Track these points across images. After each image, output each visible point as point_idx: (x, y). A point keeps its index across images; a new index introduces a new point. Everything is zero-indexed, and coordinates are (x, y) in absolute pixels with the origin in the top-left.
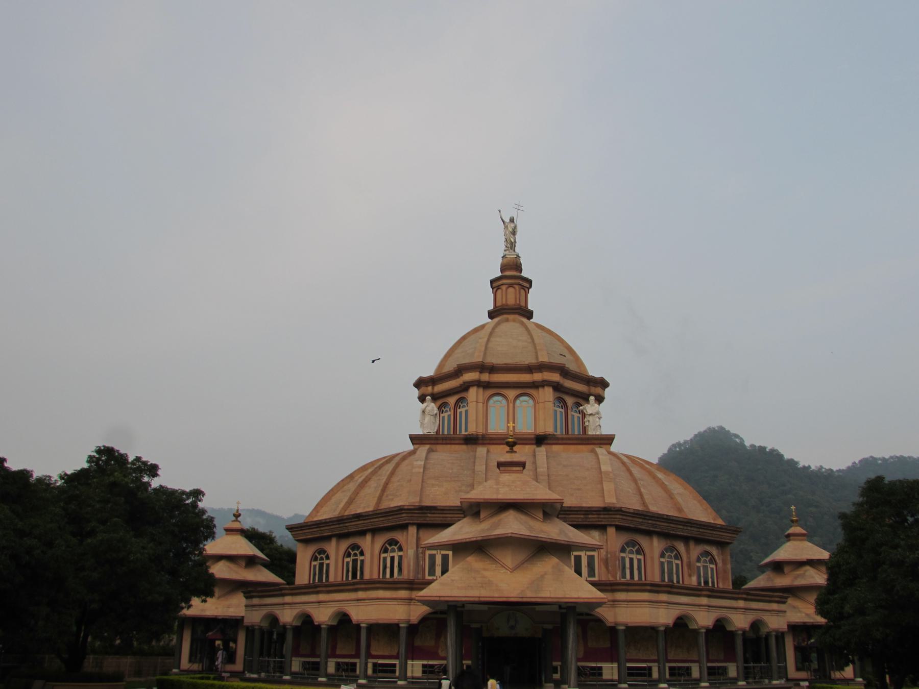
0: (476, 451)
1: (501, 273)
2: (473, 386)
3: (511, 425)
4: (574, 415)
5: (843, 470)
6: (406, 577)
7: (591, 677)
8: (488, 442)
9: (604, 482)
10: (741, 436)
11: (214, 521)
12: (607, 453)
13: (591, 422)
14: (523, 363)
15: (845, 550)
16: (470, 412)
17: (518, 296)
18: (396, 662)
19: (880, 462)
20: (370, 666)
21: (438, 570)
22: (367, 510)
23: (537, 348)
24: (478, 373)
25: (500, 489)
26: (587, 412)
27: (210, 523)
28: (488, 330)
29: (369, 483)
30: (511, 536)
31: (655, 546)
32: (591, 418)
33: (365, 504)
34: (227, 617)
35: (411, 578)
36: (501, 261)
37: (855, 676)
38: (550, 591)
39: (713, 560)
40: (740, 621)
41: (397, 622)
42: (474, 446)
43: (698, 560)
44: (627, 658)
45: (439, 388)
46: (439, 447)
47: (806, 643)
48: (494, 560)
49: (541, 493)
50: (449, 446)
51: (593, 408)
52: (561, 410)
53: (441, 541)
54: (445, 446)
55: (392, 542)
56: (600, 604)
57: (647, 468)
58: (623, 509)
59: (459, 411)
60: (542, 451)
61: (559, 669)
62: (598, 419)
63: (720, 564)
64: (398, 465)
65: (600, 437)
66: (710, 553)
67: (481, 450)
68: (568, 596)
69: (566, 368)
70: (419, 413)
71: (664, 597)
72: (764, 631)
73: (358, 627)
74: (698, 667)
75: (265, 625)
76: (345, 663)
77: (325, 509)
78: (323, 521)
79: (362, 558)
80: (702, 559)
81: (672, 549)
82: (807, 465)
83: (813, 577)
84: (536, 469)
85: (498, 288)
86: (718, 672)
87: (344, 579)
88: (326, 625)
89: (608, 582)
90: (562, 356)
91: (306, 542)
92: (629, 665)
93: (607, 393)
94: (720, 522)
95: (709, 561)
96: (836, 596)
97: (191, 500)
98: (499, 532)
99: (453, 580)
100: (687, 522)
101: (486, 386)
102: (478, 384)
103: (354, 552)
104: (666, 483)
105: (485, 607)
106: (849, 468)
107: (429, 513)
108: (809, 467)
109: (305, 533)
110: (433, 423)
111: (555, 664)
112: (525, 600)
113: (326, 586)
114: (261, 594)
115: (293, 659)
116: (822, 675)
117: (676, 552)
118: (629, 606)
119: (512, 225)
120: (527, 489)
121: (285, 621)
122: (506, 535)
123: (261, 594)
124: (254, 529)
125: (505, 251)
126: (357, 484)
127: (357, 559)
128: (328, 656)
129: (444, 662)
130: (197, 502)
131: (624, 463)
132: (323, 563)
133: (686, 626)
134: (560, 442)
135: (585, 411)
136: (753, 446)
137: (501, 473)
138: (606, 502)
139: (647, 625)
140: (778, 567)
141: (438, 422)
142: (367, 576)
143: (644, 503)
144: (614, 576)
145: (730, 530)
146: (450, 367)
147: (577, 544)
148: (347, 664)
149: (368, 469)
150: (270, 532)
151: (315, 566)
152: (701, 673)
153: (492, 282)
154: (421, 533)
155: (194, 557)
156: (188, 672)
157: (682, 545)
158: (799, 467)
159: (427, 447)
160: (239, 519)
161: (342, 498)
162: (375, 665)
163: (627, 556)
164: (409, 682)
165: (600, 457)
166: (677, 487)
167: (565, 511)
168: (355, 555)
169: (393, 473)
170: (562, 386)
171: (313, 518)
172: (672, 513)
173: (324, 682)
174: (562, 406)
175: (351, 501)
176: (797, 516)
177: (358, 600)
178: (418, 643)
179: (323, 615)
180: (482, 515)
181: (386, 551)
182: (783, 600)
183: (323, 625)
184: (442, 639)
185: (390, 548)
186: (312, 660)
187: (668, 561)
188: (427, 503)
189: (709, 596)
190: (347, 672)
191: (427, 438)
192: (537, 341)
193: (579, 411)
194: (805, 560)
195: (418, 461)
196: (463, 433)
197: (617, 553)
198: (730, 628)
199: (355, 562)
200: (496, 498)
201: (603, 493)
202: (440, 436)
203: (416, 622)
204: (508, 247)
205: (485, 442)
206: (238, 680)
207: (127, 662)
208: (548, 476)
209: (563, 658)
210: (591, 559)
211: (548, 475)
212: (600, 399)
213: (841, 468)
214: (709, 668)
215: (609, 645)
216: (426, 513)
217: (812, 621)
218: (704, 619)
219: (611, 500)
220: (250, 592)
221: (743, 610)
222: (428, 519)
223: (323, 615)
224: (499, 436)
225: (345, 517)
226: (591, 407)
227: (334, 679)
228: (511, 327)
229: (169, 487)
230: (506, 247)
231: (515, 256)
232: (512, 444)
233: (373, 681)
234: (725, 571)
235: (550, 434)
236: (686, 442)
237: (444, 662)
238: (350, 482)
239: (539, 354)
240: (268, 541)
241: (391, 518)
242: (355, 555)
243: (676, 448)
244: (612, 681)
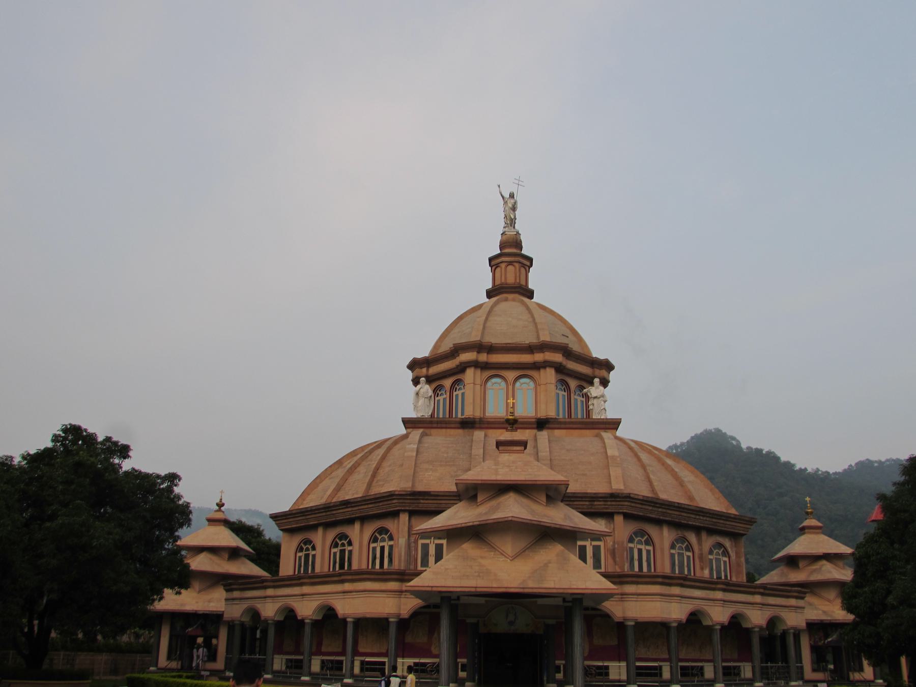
0: (473, 436)
1: (501, 250)
2: (469, 366)
3: (511, 401)
4: (578, 399)
5: (839, 473)
6: (397, 568)
7: (597, 677)
8: (486, 425)
9: (610, 468)
10: (738, 438)
11: (189, 507)
12: (613, 437)
13: (595, 405)
14: (523, 343)
15: (875, 539)
16: (466, 395)
17: (518, 275)
18: (386, 660)
19: (876, 465)
20: (357, 664)
21: (432, 559)
22: (356, 496)
23: (539, 327)
24: (475, 353)
25: (499, 470)
26: (591, 394)
27: (186, 509)
28: (486, 309)
29: (358, 469)
30: (511, 520)
31: (665, 537)
32: (595, 401)
33: (355, 490)
34: (208, 612)
35: (402, 568)
36: (500, 238)
37: (875, 677)
38: (554, 581)
39: (726, 553)
40: (757, 618)
41: (386, 616)
42: (471, 430)
43: (711, 552)
45: (434, 370)
46: (433, 431)
47: (822, 642)
48: (492, 548)
49: (544, 474)
50: (444, 430)
51: (598, 390)
52: (563, 393)
53: (434, 526)
54: (439, 430)
55: (383, 531)
56: (607, 596)
57: (656, 454)
58: (632, 496)
59: (455, 394)
60: (543, 435)
61: (562, 669)
62: (603, 402)
64: (389, 449)
65: (605, 421)
66: (722, 545)
67: (479, 434)
68: (575, 587)
69: (568, 348)
70: (413, 395)
71: (676, 590)
72: (780, 629)
73: (344, 621)
74: (713, 667)
75: (246, 619)
76: (330, 660)
77: (311, 497)
78: (309, 509)
79: (350, 548)
80: (715, 552)
81: (683, 539)
82: (803, 468)
83: (830, 572)
84: (537, 454)
85: (497, 266)
86: (734, 673)
87: (331, 570)
88: (310, 619)
89: (616, 573)
90: (565, 337)
91: (290, 531)
92: (638, 664)
93: (612, 376)
94: (733, 511)
95: (722, 553)
96: (866, 589)
97: (166, 484)
98: (499, 515)
99: (446, 569)
102: (476, 365)
103: (342, 542)
104: (677, 470)
105: (482, 600)
106: (845, 470)
107: (423, 499)
108: (806, 469)
109: (290, 522)
110: (428, 406)
111: (558, 662)
112: (526, 591)
113: (310, 577)
114: (241, 587)
115: (276, 656)
116: (840, 675)
117: (687, 543)
118: (639, 599)
119: (512, 201)
120: (529, 470)
121: (267, 615)
122: (506, 519)
123: (241, 587)
124: (242, 522)
125: (504, 227)
126: (346, 471)
127: (345, 549)
128: (312, 654)
129: (436, 660)
130: (173, 488)
131: (631, 448)
132: (309, 554)
133: (699, 622)
134: (563, 426)
135: (589, 394)
136: (749, 448)
137: (500, 453)
138: (613, 488)
139: (659, 620)
140: (792, 561)
141: (433, 405)
142: (355, 566)
143: (653, 491)
144: (622, 567)
145: (744, 520)
146: (447, 346)
147: (584, 530)
148: (332, 661)
149: (357, 454)
150: (258, 525)
152: (715, 673)
153: (491, 260)
154: (413, 520)
155: (168, 545)
156: (165, 670)
158: (795, 469)
159: (421, 430)
161: (330, 485)
162: (362, 663)
165: (606, 441)
166: (688, 475)
167: (569, 497)
168: (343, 545)
169: (384, 457)
170: (565, 367)
171: (299, 507)
172: (683, 501)
173: (881, 683)
174: (564, 389)
175: (338, 489)
176: (812, 508)
177: (344, 592)
178: (409, 639)
179: (307, 609)
180: (479, 499)
181: (375, 540)
183: (307, 619)
184: (436, 635)
185: (380, 538)
186: (295, 658)
187: (678, 553)
188: (420, 488)
189: (724, 590)
190: (334, 669)
191: (420, 421)
192: (537, 320)
193: (583, 394)
194: (822, 554)
195: (411, 445)
196: (459, 416)
198: (745, 625)
199: (342, 552)
200: (495, 479)
201: (610, 479)
202: (435, 419)
203: (406, 616)
204: (508, 224)
205: (483, 426)
206: (217, 678)
207: (102, 660)
208: (550, 453)
209: (568, 657)
210: (596, 549)
211: (551, 460)
212: (605, 383)
213: (837, 471)
214: (724, 668)
217: (829, 618)
218: (719, 615)
219: (618, 486)
220: (231, 584)
221: (761, 606)
222: (421, 505)
223: (307, 609)
224: (499, 420)
225: (332, 505)
226: (595, 390)
227: (318, 679)
228: (511, 306)
229: (143, 470)
230: (506, 223)
231: (515, 233)
232: (512, 423)
233: (360, 680)
234: (739, 565)
235: (551, 418)
236: (682, 444)
237: (436, 660)
238: (338, 468)
239: (541, 333)
240: (256, 535)
241: (381, 504)
242: (343, 545)
243: (672, 450)
244: (619, 681)
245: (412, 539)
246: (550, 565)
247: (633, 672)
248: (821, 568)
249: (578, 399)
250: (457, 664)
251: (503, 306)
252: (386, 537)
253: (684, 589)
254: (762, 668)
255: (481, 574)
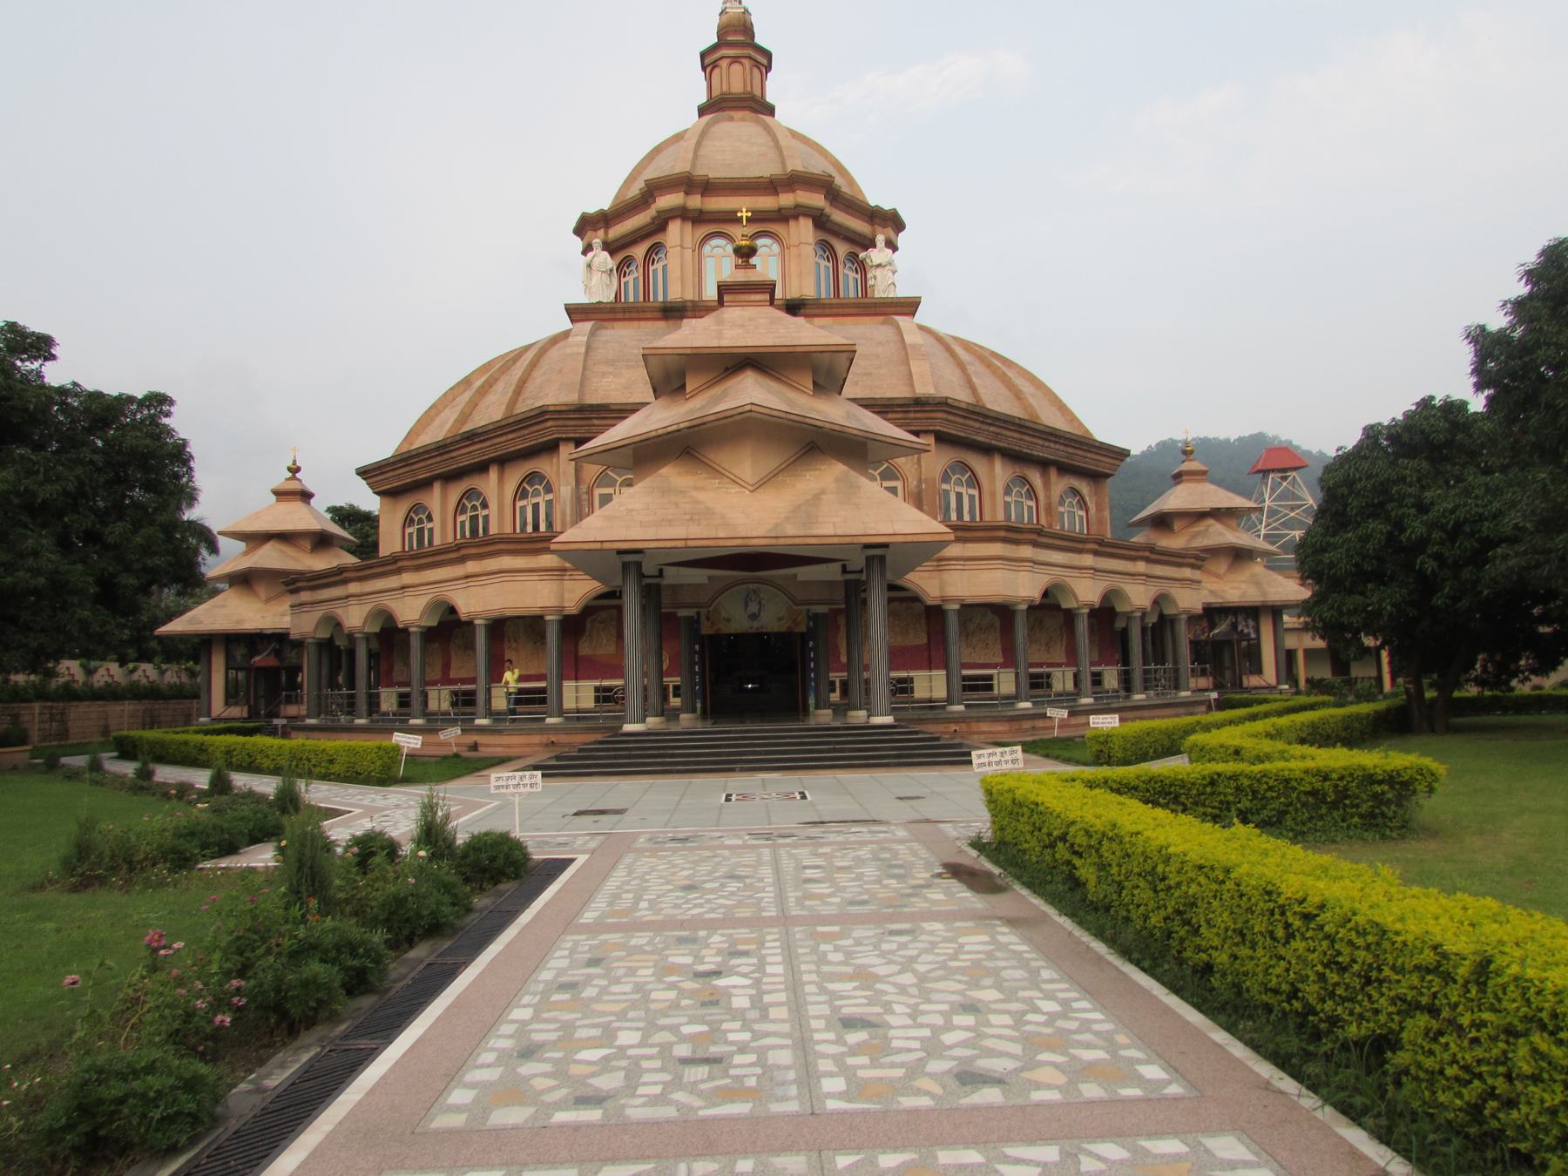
2: (674, 218)
31: (997, 473)
32: (878, 272)
37: (1279, 682)
39: (1083, 504)
40: (1139, 596)
44: (964, 661)
48: (716, 472)
52: (826, 263)
55: (533, 477)
58: (950, 401)
59: (651, 268)
63: (1093, 511)
68: (874, 532)
71: (1026, 551)
75: (324, 634)
83: (1221, 534)
85: (714, 65)
88: (418, 626)
92: (965, 672)
93: (902, 239)
100: (1051, 434)
101: (697, 218)
102: (683, 214)
107: (597, 418)
113: (412, 558)
134: (827, 311)
140: (1162, 522)
146: (635, 190)
151: (411, 535)
153: (703, 55)
157: (1038, 475)
160: (297, 475)
163: (952, 488)
164: (567, 718)
177: (467, 577)
179: (411, 611)
180: (690, 386)
181: (524, 495)
182: (1199, 563)
189: (1096, 553)
197: (938, 481)
203: (574, 611)
215: (925, 641)
216: (591, 418)
218: (1087, 592)
223: (411, 611)
241: (526, 432)
245: (584, 488)
246: (824, 497)
247: (957, 684)
248: (1206, 530)
249: (849, 275)
250: (665, 689)
251: (725, 126)
252: (540, 488)
253: (1038, 550)
254: (1146, 672)
255: (696, 517)
